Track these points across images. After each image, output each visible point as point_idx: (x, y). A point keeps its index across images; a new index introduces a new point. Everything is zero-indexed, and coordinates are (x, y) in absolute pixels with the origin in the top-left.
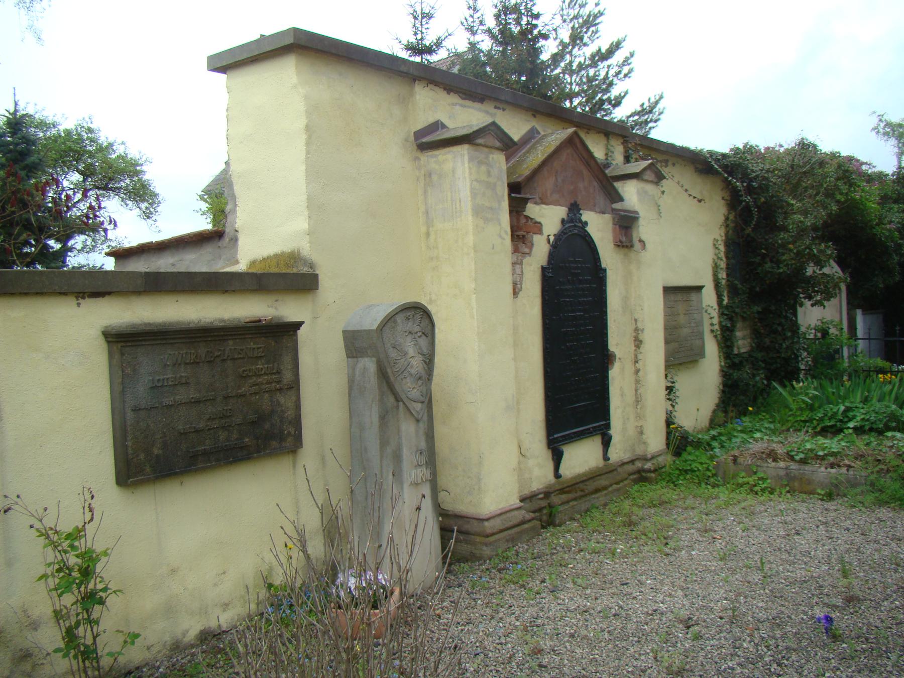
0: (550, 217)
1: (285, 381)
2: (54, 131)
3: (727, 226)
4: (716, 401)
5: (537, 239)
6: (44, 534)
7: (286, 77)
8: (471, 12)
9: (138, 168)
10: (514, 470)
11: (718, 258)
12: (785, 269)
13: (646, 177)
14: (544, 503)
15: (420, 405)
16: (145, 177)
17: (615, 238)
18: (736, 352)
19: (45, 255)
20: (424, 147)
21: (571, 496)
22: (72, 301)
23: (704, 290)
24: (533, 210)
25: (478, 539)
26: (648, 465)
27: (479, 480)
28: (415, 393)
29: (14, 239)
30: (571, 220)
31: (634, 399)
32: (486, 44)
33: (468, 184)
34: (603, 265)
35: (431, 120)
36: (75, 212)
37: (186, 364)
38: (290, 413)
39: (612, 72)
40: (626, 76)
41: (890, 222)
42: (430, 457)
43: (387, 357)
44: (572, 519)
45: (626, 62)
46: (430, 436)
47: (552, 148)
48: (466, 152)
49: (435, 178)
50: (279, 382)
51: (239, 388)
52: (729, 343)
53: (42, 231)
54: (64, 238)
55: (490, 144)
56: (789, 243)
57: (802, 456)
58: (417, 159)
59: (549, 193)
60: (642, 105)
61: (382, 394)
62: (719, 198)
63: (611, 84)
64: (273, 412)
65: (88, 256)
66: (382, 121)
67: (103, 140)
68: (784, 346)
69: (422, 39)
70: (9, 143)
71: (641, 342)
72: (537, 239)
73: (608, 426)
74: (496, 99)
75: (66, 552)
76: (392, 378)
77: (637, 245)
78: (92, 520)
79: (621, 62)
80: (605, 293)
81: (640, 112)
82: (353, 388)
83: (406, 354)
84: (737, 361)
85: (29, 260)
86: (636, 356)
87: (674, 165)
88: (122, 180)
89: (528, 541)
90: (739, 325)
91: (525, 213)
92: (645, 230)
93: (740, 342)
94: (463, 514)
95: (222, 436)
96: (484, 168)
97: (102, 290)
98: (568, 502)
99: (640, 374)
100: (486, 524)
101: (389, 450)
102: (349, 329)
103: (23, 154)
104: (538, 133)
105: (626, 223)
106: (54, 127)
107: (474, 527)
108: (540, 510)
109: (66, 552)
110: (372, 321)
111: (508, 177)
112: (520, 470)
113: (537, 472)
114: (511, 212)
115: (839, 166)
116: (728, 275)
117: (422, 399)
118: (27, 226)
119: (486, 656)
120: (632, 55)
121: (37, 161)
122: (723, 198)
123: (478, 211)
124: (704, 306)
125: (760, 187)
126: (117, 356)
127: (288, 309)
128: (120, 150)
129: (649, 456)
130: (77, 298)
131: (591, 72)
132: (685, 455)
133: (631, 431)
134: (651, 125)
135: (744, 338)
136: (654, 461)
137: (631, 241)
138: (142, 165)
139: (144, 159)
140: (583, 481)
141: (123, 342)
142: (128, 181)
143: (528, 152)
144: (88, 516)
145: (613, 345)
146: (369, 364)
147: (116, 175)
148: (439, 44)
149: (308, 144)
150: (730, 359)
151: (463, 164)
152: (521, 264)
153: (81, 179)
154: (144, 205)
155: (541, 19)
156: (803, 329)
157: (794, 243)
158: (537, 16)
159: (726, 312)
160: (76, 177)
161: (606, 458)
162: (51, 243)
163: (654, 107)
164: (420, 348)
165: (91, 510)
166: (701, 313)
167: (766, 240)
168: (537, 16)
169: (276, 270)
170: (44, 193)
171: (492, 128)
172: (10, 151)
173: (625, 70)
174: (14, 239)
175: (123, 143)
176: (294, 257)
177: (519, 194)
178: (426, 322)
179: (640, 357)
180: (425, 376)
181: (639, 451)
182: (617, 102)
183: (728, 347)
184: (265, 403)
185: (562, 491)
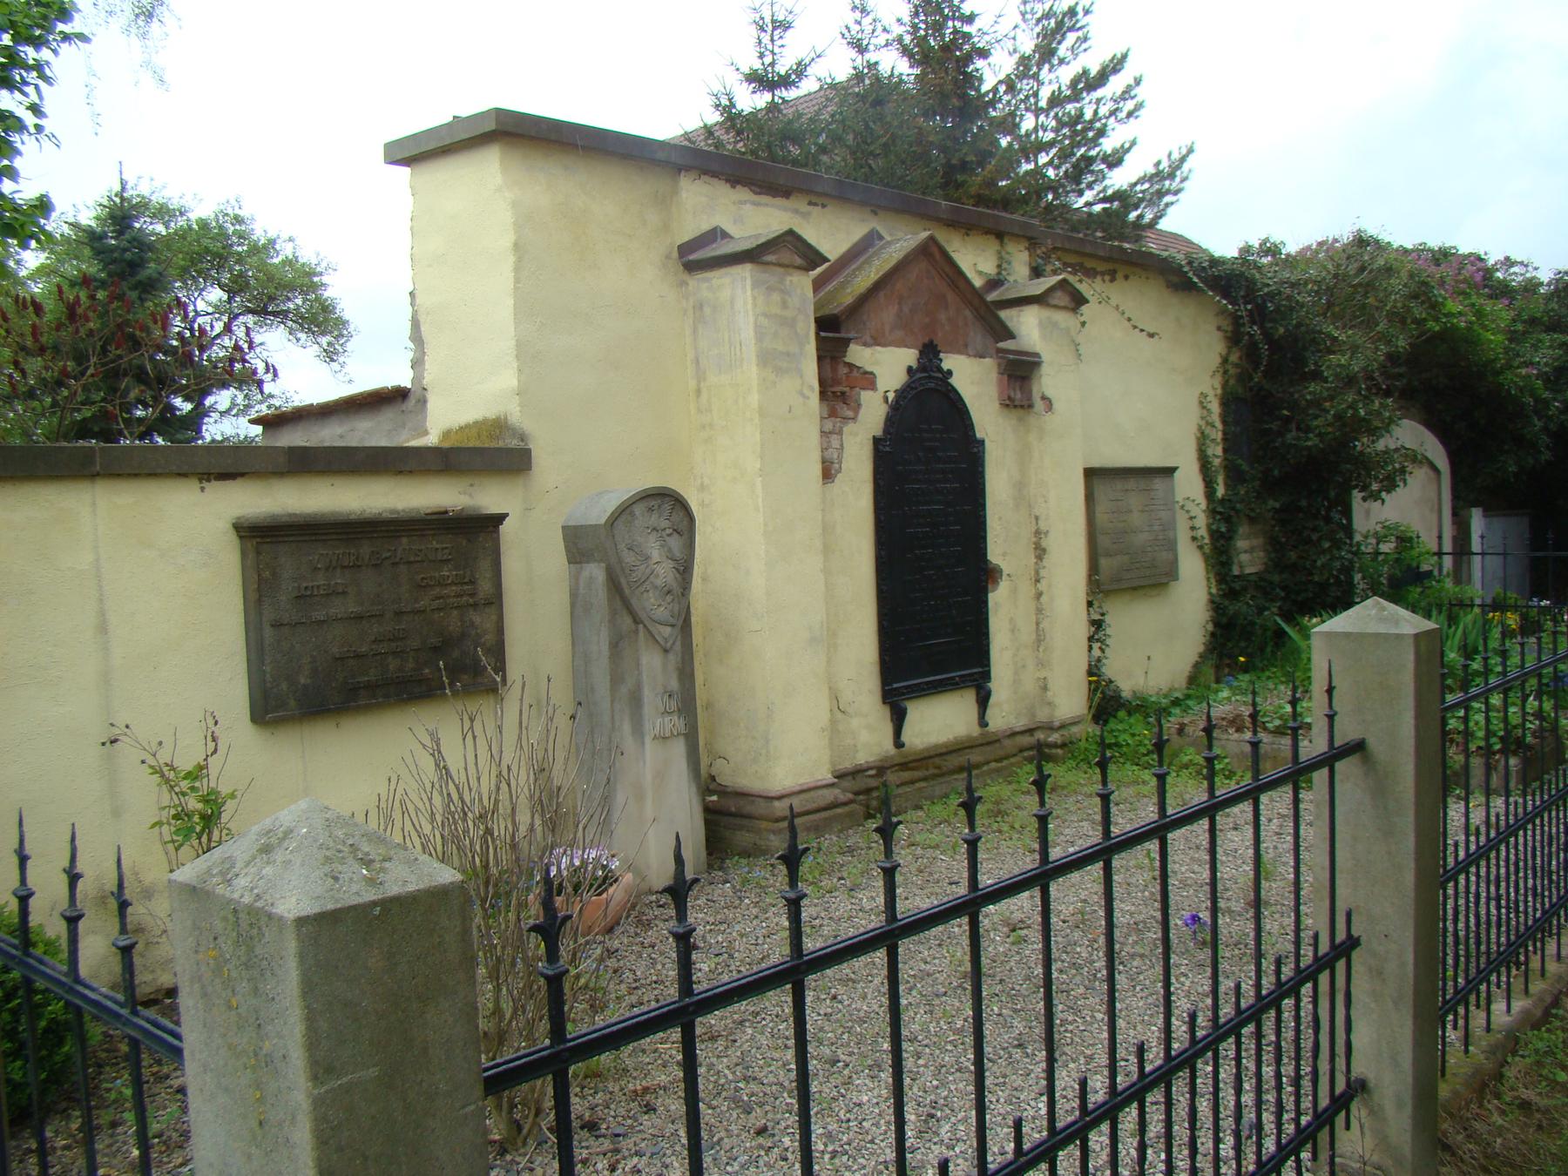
0: (888, 366)
1: (481, 595)
2: (182, 222)
3: (1225, 372)
4: (1201, 649)
5: (866, 396)
6: (156, 771)
7: (487, 171)
8: (858, 15)
9: (316, 279)
10: (823, 730)
11: (1208, 423)
12: (1316, 440)
13: (1055, 302)
14: (873, 783)
15: (669, 629)
16: (327, 294)
17: (1001, 393)
18: (1236, 571)
19: (168, 422)
20: (692, 267)
21: (916, 774)
22: (194, 485)
23: (1177, 474)
24: (860, 355)
25: (764, 825)
26: (1055, 737)
27: (767, 741)
28: (661, 613)
29: (122, 397)
30: (922, 368)
31: (1034, 636)
32: (895, 64)
33: (751, 319)
34: (979, 435)
35: (706, 227)
36: (217, 352)
37: (344, 567)
38: (489, 638)
39: (1103, 111)
40: (1130, 115)
41: (1530, 364)
42: (686, 702)
43: (620, 561)
44: (918, 807)
45: (1126, 94)
46: (686, 673)
47: (893, 262)
48: (748, 275)
49: (707, 310)
50: (472, 595)
51: (416, 601)
52: (1224, 559)
53: (161, 383)
54: (198, 394)
55: (786, 262)
56: (1325, 400)
57: (1277, 722)
58: (683, 283)
59: (887, 328)
60: (1158, 164)
61: (613, 613)
62: (1212, 328)
63: (1102, 133)
64: (463, 636)
65: (227, 421)
66: (625, 236)
67: (259, 233)
68: (1319, 563)
69: (772, 64)
70: (116, 248)
71: (1044, 550)
72: (866, 396)
73: (986, 676)
74: (809, 192)
75: (184, 794)
76: (627, 591)
77: (1039, 405)
78: (215, 751)
79: (1119, 93)
80: (983, 477)
81: (1152, 176)
82: (578, 606)
83: (648, 558)
84: (1237, 586)
85: (142, 429)
86: (1037, 572)
87: (1126, 277)
88: (289, 299)
89: (841, 831)
90: (1243, 529)
91: (847, 360)
92: (1049, 381)
93: (1244, 557)
94: (745, 790)
95: (393, 663)
96: (776, 297)
97: (232, 470)
98: (912, 782)
99: (1044, 599)
100: (777, 804)
101: (624, 690)
102: (571, 523)
103: (134, 266)
104: (881, 238)
105: (1019, 372)
106: (182, 214)
107: (760, 808)
108: (868, 791)
109: (184, 794)
110: (599, 513)
111: (816, 310)
112: (833, 729)
113: (864, 737)
114: (820, 359)
115: (1411, 276)
116: (1225, 451)
117: (672, 621)
118: (141, 376)
119: (731, 956)
120: (1138, 82)
121: (155, 275)
122: (1219, 328)
123: (765, 359)
124: (1179, 498)
125: (1277, 310)
126: (251, 555)
127: (488, 497)
128: (286, 250)
129: (1057, 724)
130: (201, 480)
131: (1071, 108)
132: (1112, 724)
133: (1029, 685)
134: (1168, 199)
135: (1251, 550)
136: (1064, 732)
137: (1029, 397)
138: (321, 274)
139: (324, 265)
140: (941, 755)
141: (259, 537)
142: (299, 301)
143: (858, 268)
144: (211, 745)
145: (997, 551)
146: (595, 572)
147: (283, 292)
148: (800, 70)
149: (517, 269)
150: (1227, 583)
151: (744, 287)
152: (840, 433)
153: (225, 297)
154: (324, 340)
155: (978, 24)
156: (1358, 538)
157: (1331, 398)
158: (970, 19)
159: (1220, 509)
160: (216, 294)
161: (983, 723)
162: (178, 402)
163: (1179, 167)
164: (670, 550)
165: (214, 740)
166: (1172, 510)
167: (1292, 394)
168: (970, 19)
169: (478, 444)
170: (166, 325)
171: (789, 238)
172: (114, 261)
173: (1129, 105)
174: (122, 397)
175: (291, 240)
176: (498, 426)
177: (832, 332)
178: (678, 516)
179: (1043, 573)
180: (677, 590)
181: (1042, 715)
182: (1114, 160)
183: (1223, 564)
184: (453, 623)
185: (903, 766)
